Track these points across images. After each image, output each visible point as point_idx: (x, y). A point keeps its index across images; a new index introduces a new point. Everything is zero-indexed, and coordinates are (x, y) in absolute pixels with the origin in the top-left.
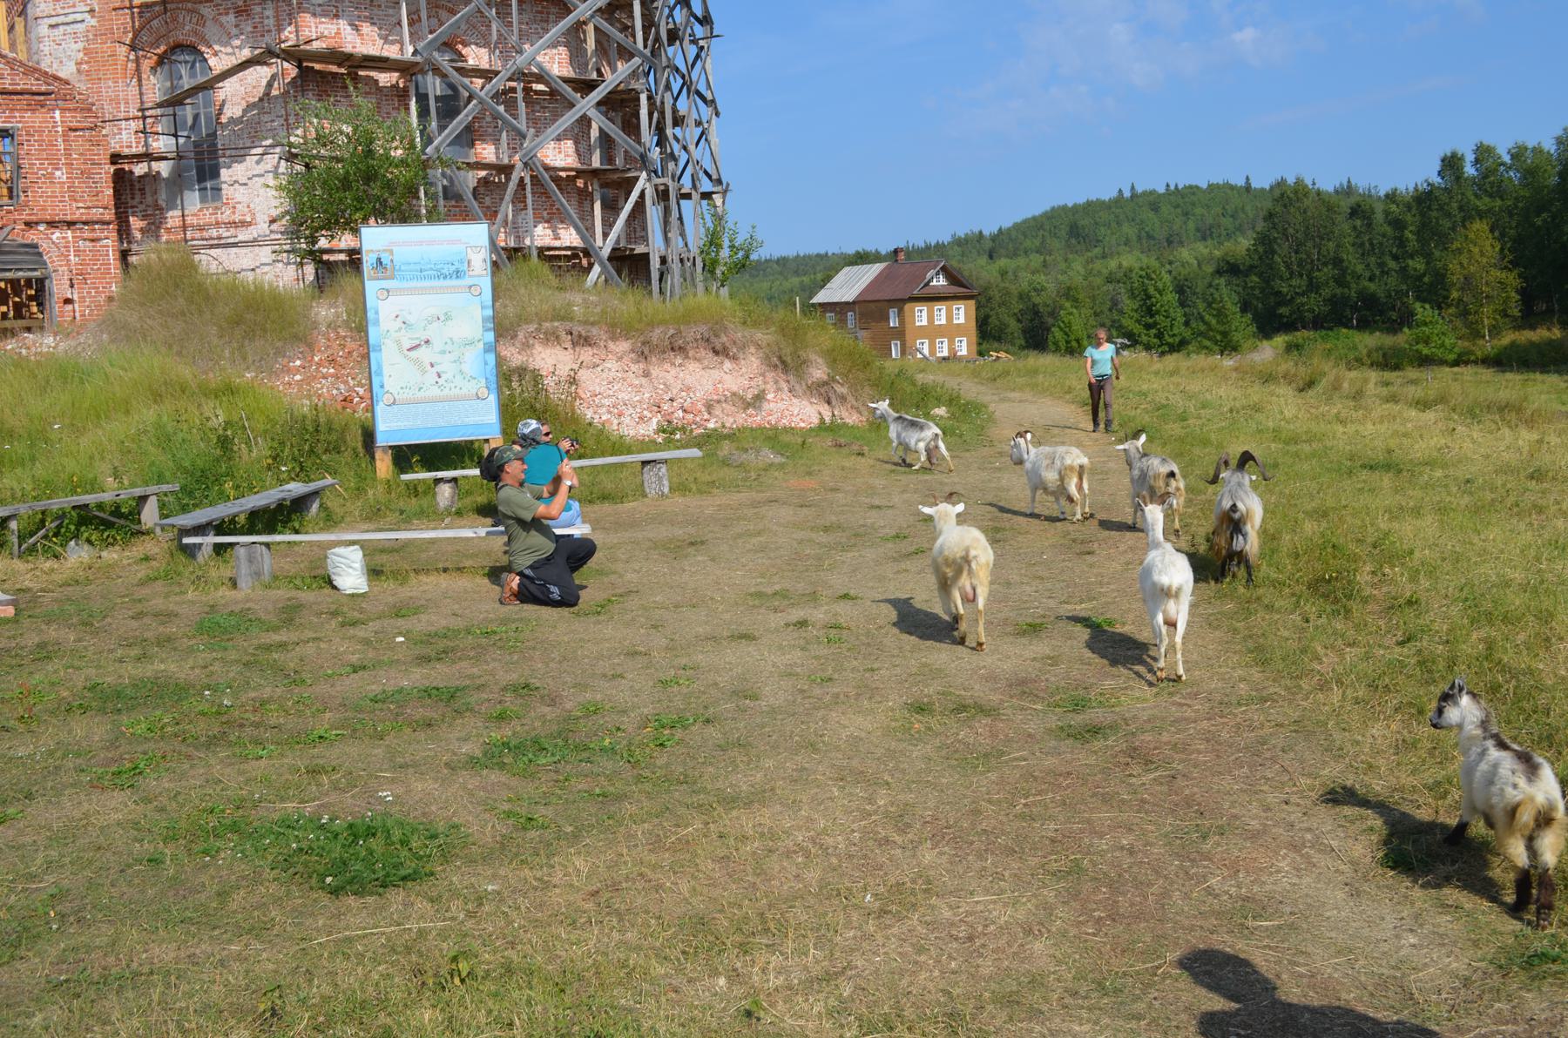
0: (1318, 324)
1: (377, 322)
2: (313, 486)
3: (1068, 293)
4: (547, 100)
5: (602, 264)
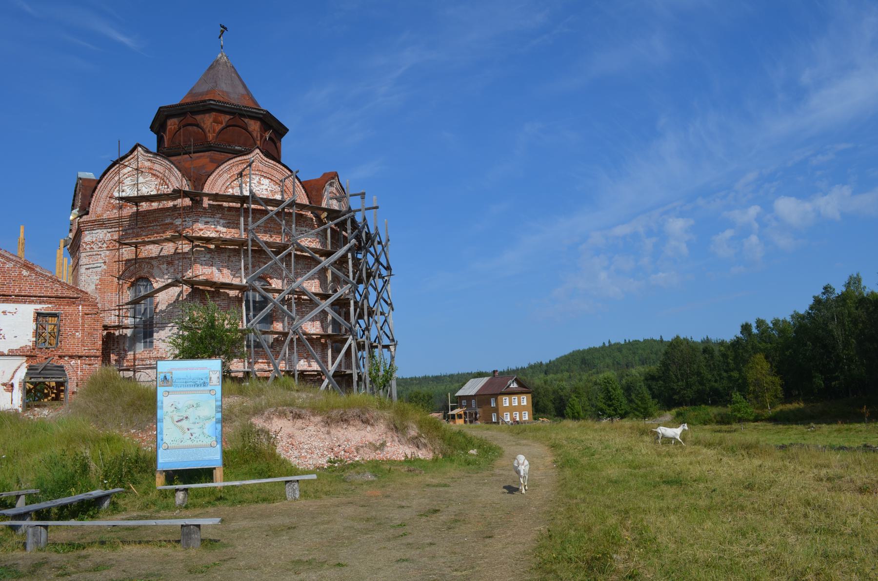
0: (693, 403)
1: (162, 408)
2: (107, 492)
3: (575, 390)
4: (304, 303)
5: (329, 378)
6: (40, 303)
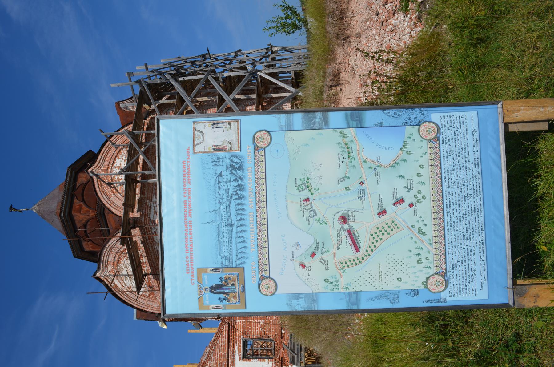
1: (312, 297)
6: (234, 356)
